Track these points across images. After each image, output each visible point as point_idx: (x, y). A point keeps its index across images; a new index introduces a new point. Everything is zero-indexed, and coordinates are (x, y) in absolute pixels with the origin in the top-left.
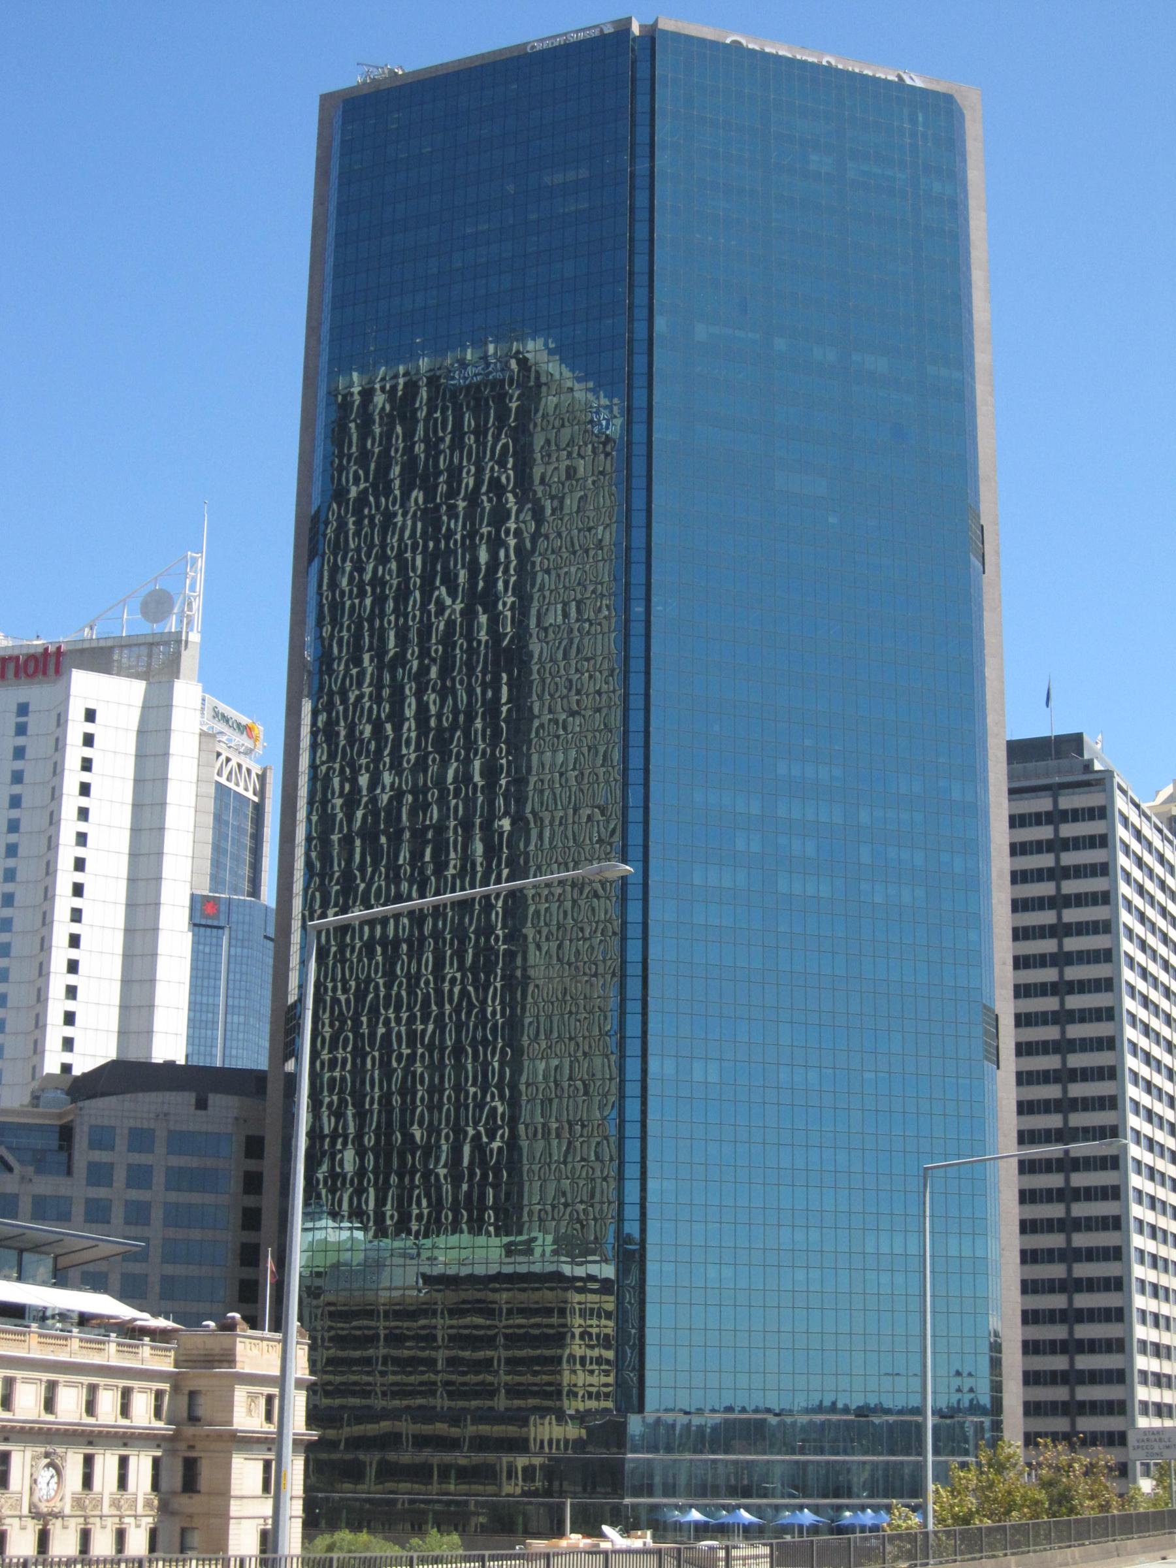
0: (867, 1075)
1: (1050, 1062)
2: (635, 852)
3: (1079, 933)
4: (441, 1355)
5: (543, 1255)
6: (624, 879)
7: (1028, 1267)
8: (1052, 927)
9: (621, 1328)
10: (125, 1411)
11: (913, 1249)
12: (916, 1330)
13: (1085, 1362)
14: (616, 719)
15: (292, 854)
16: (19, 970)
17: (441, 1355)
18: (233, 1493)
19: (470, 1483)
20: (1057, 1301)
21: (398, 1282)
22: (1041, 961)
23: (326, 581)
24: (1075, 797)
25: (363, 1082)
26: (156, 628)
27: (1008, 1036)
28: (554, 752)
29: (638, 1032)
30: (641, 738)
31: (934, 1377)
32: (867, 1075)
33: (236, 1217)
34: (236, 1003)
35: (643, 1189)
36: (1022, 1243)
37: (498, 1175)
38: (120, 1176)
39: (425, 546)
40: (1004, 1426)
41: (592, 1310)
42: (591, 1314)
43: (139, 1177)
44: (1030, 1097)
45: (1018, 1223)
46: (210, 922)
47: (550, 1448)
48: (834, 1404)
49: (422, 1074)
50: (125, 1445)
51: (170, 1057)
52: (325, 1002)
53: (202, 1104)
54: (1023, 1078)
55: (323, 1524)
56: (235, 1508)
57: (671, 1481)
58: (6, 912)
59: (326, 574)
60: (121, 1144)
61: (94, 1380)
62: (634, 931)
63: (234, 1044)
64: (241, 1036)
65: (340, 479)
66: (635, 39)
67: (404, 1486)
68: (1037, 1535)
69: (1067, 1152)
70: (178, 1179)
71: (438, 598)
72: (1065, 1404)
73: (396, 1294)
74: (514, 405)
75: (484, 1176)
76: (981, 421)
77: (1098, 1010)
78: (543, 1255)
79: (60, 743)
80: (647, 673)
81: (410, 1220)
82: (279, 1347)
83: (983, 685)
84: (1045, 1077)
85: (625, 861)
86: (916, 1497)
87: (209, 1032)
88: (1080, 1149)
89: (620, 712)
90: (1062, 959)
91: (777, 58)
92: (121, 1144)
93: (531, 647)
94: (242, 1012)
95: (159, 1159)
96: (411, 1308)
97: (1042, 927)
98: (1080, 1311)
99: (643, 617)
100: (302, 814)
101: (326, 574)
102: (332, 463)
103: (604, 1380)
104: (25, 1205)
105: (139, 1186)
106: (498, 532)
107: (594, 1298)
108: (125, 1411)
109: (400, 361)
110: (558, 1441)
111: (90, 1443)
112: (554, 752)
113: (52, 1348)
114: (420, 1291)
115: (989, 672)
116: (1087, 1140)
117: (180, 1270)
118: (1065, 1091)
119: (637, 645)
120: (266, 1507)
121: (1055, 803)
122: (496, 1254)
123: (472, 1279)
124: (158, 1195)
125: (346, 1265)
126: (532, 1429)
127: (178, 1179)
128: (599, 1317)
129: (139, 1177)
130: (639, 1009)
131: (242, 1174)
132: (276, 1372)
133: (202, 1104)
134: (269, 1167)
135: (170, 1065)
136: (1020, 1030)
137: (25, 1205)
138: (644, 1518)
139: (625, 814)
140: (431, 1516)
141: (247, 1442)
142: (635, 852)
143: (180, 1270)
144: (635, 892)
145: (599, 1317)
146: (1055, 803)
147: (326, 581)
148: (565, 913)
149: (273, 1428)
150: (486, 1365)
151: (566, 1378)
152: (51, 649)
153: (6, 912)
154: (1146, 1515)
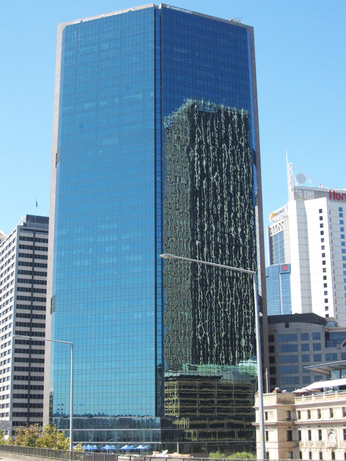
0: (88, 316)
1: (34, 365)
2: (159, 262)
3: (26, 314)
4: (216, 400)
5: (186, 370)
6: (162, 253)
7: (43, 331)
8: (35, 275)
9: (163, 391)
10: (309, 417)
11: (76, 365)
12: (75, 388)
13: (25, 383)
14: (165, 211)
15: (261, 260)
16: (341, 279)
17: (216, 400)
18: (277, 449)
19: (207, 438)
20: (32, 401)
21: (228, 378)
22: (38, 282)
23: (251, 169)
24: (26, 234)
25: (239, 319)
26: (301, 185)
27: (48, 305)
28: (183, 221)
29: (158, 289)
30: (157, 174)
31: (69, 405)
32: (88, 316)
33: (277, 360)
34: (277, 295)
35: (156, 328)
36: (42, 419)
37: (199, 346)
38: (311, 347)
39: (222, 160)
40: (49, 420)
41: (171, 386)
42: (171, 387)
43: (305, 347)
44: (41, 355)
45: (45, 371)
46: (285, 272)
47: (183, 427)
48: (99, 414)
49: (222, 319)
50: (309, 427)
51: (297, 312)
52: (251, 322)
53: (287, 326)
54: (44, 291)
55: (250, 450)
56: (276, 445)
57: (147, 437)
58: (345, 262)
59: (251, 171)
60: (311, 338)
61: (318, 408)
62: (159, 274)
63: (277, 308)
64: (275, 306)
65: (247, 141)
66: (160, 10)
67: (226, 439)
68: (39, 452)
69: (31, 339)
70: (294, 348)
71: (218, 181)
72: (33, 344)
73: (229, 382)
74: (196, 118)
75: (203, 347)
76: (57, 122)
77: (20, 343)
78: (186, 370)
79: (332, 257)
80: (156, 204)
81: (225, 358)
82: (264, 405)
83: (56, 207)
84: (38, 291)
85: (162, 258)
86: (74, 431)
87: (284, 295)
88: (27, 338)
89: (164, 212)
90: (32, 282)
91: (118, 15)
92: (311, 338)
93: (190, 190)
94: (275, 303)
95: (300, 353)
96: (224, 386)
97: (38, 275)
98: (30, 291)
99: (157, 177)
100: (258, 255)
101: (251, 171)
102: (249, 136)
103: (167, 407)
104: (339, 356)
105: (306, 350)
106: (200, 156)
107: (171, 382)
108: (309, 417)
109: (229, 105)
110: (181, 425)
111: (319, 426)
112: (183, 221)
113: (331, 398)
114: (222, 381)
115: (54, 197)
116: (24, 335)
117: (293, 375)
118: (34, 252)
119: (159, 147)
120: (267, 445)
121: (34, 235)
122: (200, 370)
123: (207, 377)
124: (300, 342)
125: (244, 373)
126: (188, 424)
127: (294, 348)
128: (169, 388)
129: (305, 347)
130: (157, 131)
131: (276, 373)
132: (264, 398)
133: (287, 326)
134: (267, 354)
135: (297, 315)
136: (44, 306)
137: (339, 356)
138: (155, 448)
139: (162, 240)
140: (219, 448)
141: (273, 426)
142: (159, 262)
143: (293, 375)
144: (159, 251)
145: (169, 388)
146: (34, 235)
147: (251, 169)
148: (180, 269)
149: (265, 411)
150: (202, 403)
151: (178, 406)
152: (332, 191)
153: (345, 262)
154: (6, 446)
